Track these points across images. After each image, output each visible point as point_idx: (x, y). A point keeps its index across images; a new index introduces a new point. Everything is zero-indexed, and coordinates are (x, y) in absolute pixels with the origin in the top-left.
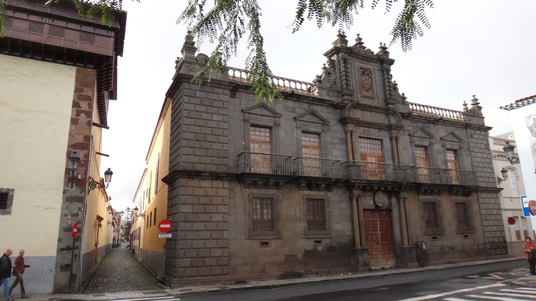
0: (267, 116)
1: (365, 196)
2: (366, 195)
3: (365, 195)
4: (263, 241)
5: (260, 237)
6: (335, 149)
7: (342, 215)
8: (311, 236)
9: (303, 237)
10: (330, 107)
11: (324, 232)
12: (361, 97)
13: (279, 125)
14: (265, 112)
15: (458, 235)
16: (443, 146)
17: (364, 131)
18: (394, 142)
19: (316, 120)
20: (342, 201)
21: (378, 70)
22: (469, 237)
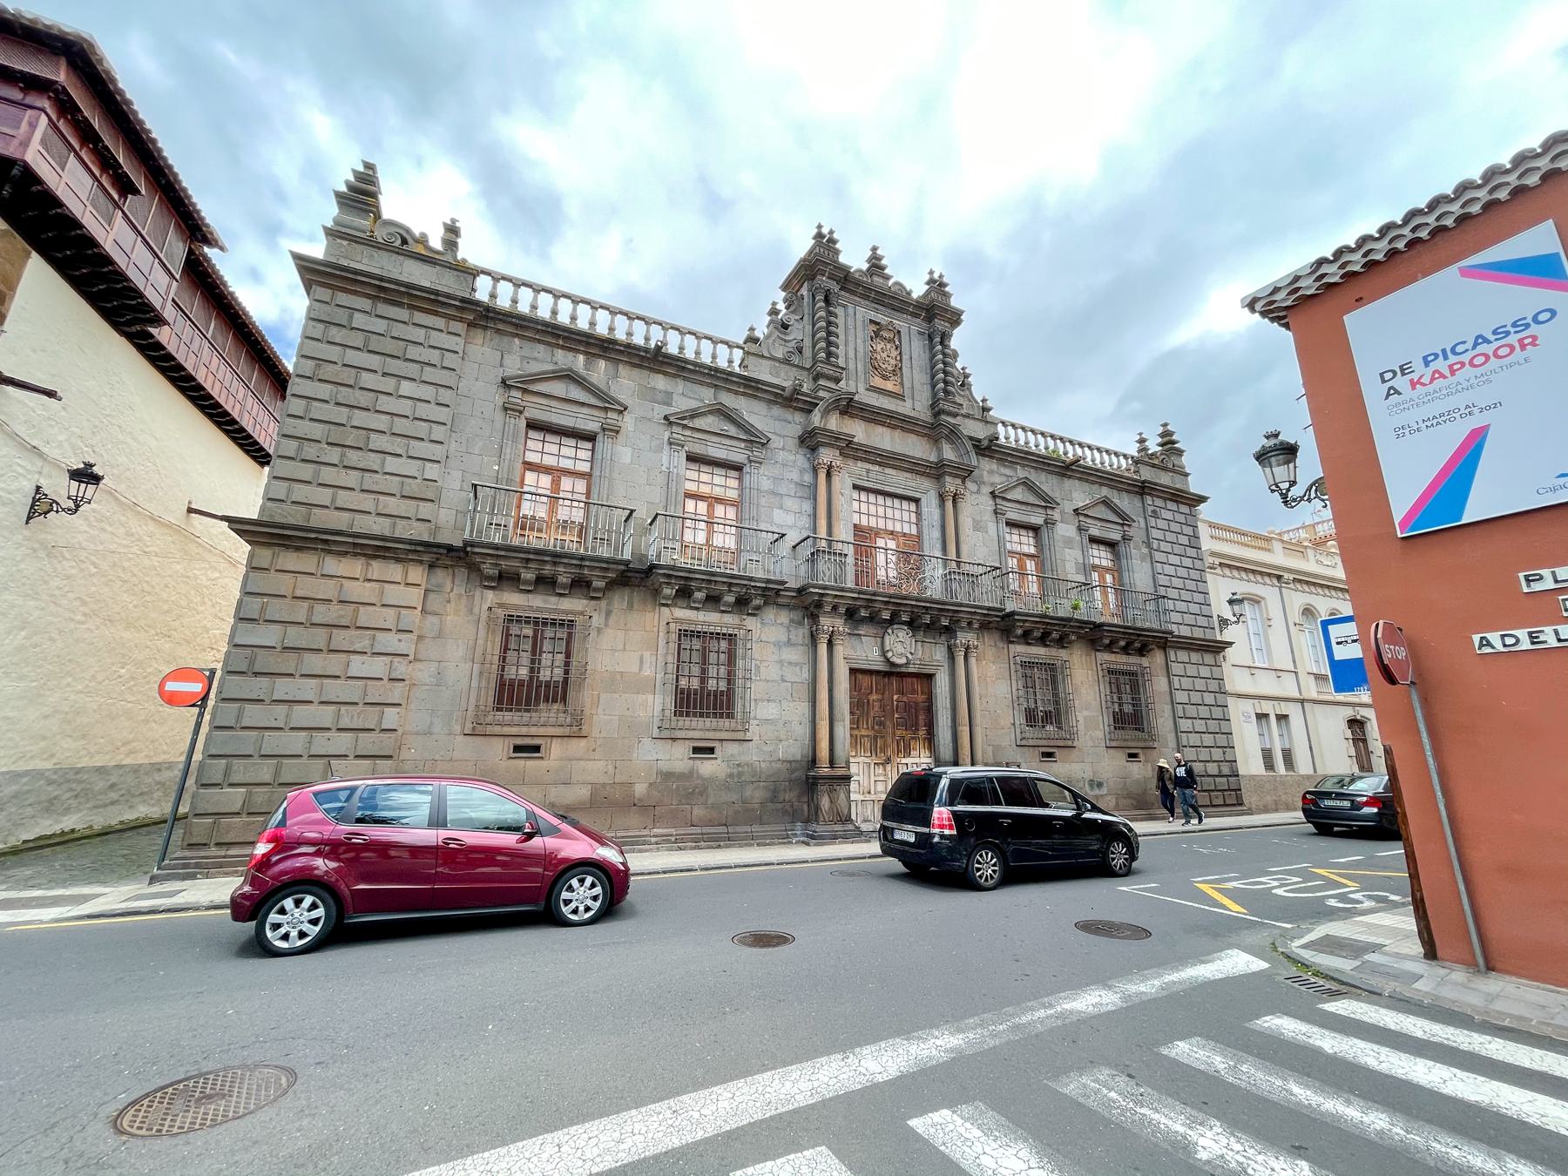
0: (583, 404)
1: (860, 635)
2: (861, 632)
3: (856, 632)
4: (519, 742)
5: (514, 730)
6: (781, 508)
7: (783, 681)
8: (497, 730)
9: (656, 733)
10: (776, 403)
11: (725, 723)
12: (867, 389)
13: (617, 432)
14: (576, 393)
15: (1111, 751)
16: (1080, 529)
17: (868, 471)
18: (949, 504)
19: (733, 431)
20: (789, 643)
21: (920, 333)
22: (1142, 758)
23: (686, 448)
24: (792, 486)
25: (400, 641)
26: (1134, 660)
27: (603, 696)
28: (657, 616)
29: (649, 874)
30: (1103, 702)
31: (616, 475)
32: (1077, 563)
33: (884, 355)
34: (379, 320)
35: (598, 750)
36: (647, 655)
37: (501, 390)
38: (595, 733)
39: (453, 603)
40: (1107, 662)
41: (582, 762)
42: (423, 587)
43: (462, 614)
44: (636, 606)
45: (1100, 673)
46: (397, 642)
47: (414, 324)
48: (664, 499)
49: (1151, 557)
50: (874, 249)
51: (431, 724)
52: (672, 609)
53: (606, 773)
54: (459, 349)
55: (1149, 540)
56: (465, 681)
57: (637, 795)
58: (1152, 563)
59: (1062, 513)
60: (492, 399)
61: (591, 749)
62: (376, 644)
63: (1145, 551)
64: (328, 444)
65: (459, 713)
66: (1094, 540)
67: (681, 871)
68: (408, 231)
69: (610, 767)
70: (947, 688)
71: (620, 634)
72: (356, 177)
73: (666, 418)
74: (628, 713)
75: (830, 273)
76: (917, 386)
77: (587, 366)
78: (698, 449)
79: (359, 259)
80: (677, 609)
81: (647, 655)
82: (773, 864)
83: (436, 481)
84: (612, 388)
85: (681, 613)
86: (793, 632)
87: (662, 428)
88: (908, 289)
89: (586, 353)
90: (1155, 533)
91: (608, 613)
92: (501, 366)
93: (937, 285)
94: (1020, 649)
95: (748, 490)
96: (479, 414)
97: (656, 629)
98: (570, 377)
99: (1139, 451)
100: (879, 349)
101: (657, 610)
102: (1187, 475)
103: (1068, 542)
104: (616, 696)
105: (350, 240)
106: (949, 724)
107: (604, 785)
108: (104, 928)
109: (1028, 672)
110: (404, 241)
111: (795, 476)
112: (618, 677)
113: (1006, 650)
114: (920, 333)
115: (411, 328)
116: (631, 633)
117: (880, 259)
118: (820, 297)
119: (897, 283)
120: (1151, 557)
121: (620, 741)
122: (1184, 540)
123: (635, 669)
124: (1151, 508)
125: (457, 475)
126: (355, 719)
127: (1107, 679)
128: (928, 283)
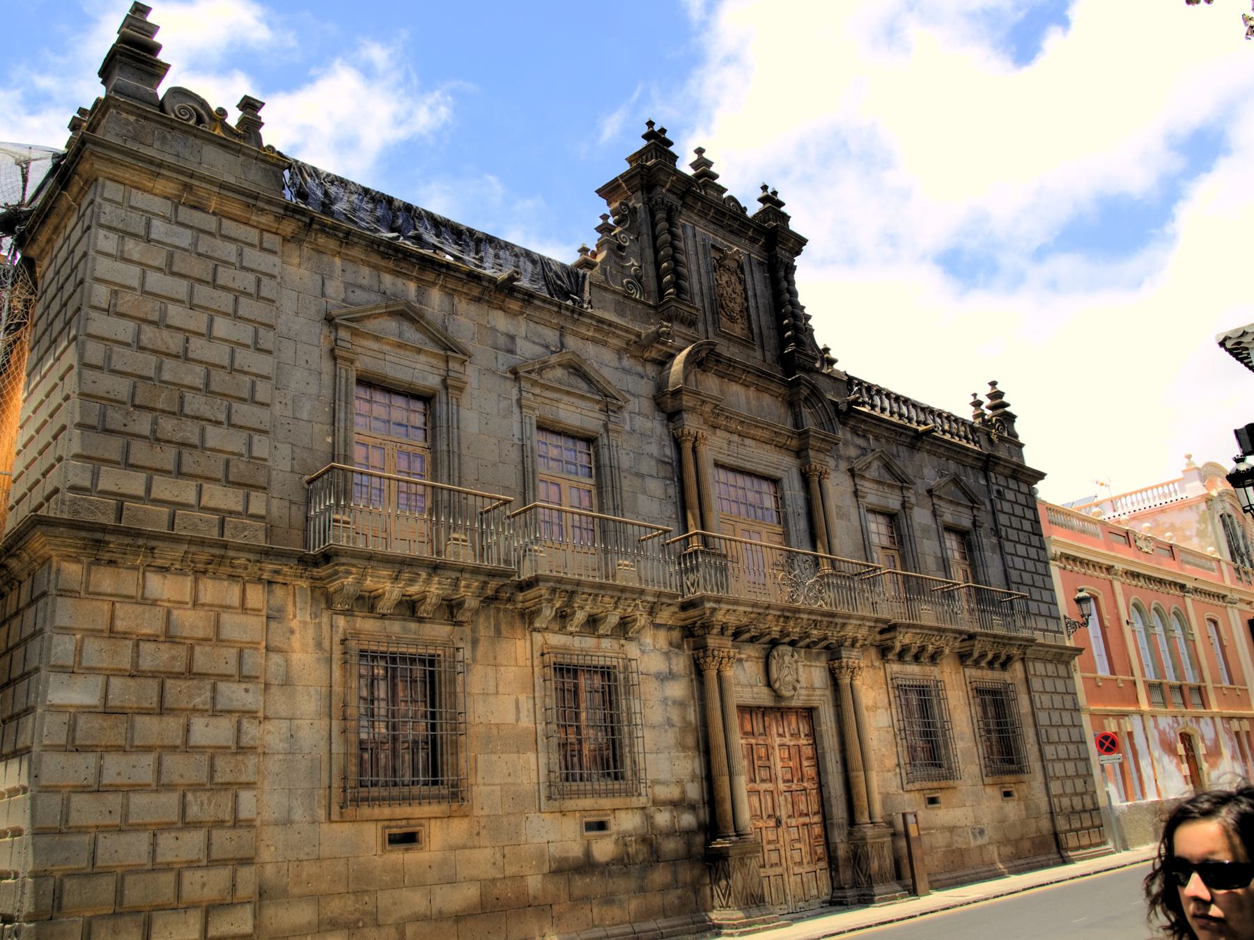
14: (412, 335)
23: (537, 412)
24: (653, 463)
25: (247, 691)
26: (928, 669)
27: (481, 758)
28: (528, 643)
29: (1024, 890)
30: (976, 730)
31: (464, 451)
32: (936, 557)
33: (730, 290)
34: (182, 229)
35: (483, 832)
36: (522, 698)
37: (326, 330)
38: (477, 812)
39: (297, 635)
40: (556, 650)
41: (467, 851)
42: (264, 613)
43: (310, 650)
44: (504, 632)
45: (970, 693)
46: (243, 692)
47: (221, 235)
48: (520, 483)
49: (1001, 548)
50: (700, 151)
51: (290, 810)
52: (546, 634)
53: (494, 864)
54: (276, 271)
55: (996, 526)
56: (323, 745)
57: (530, 891)
58: (1002, 555)
59: (916, 493)
60: (316, 343)
61: (475, 832)
62: (219, 697)
63: (994, 540)
64: (135, 406)
65: (321, 791)
66: (949, 529)
67: (903, 919)
68: (203, 104)
69: (498, 856)
70: (834, 726)
71: (490, 671)
72: (600, 232)
73: (514, 372)
74: (510, 780)
75: (672, 186)
76: (765, 331)
77: (421, 293)
78: (548, 412)
79: (149, 142)
80: (550, 635)
81: (522, 698)
82: (844, 932)
83: (265, 460)
84: (450, 328)
85: (556, 640)
86: (674, 661)
87: (509, 384)
88: (743, 206)
89: (419, 280)
90: (1003, 519)
91: (475, 643)
92: (323, 295)
93: (771, 201)
94: (895, 667)
95: (608, 469)
96: (304, 363)
97: (529, 662)
98: (408, 315)
99: (976, 416)
100: (723, 282)
101: (528, 637)
102: (1021, 446)
103: (926, 530)
104: (494, 757)
105: (140, 116)
106: (840, 770)
107: (494, 880)
108: (1019, 899)
109: (569, 681)
110: (200, 120)
111: (653, 449)
112: (495, 731)
113: (882, 671)
114: (760, 264)
115: (219, 242)
116: (503, 669)
117: (709, 164)
118: (661, 215)
119: (731, 198)
120: (1001, 548)
121: (505, 820)
122: (1027, 526)
123: (510, 718)
124: (995, 487)
125: (285, 450)
126: (206, 806)
127: (978, 700)
128: (646, 137)
